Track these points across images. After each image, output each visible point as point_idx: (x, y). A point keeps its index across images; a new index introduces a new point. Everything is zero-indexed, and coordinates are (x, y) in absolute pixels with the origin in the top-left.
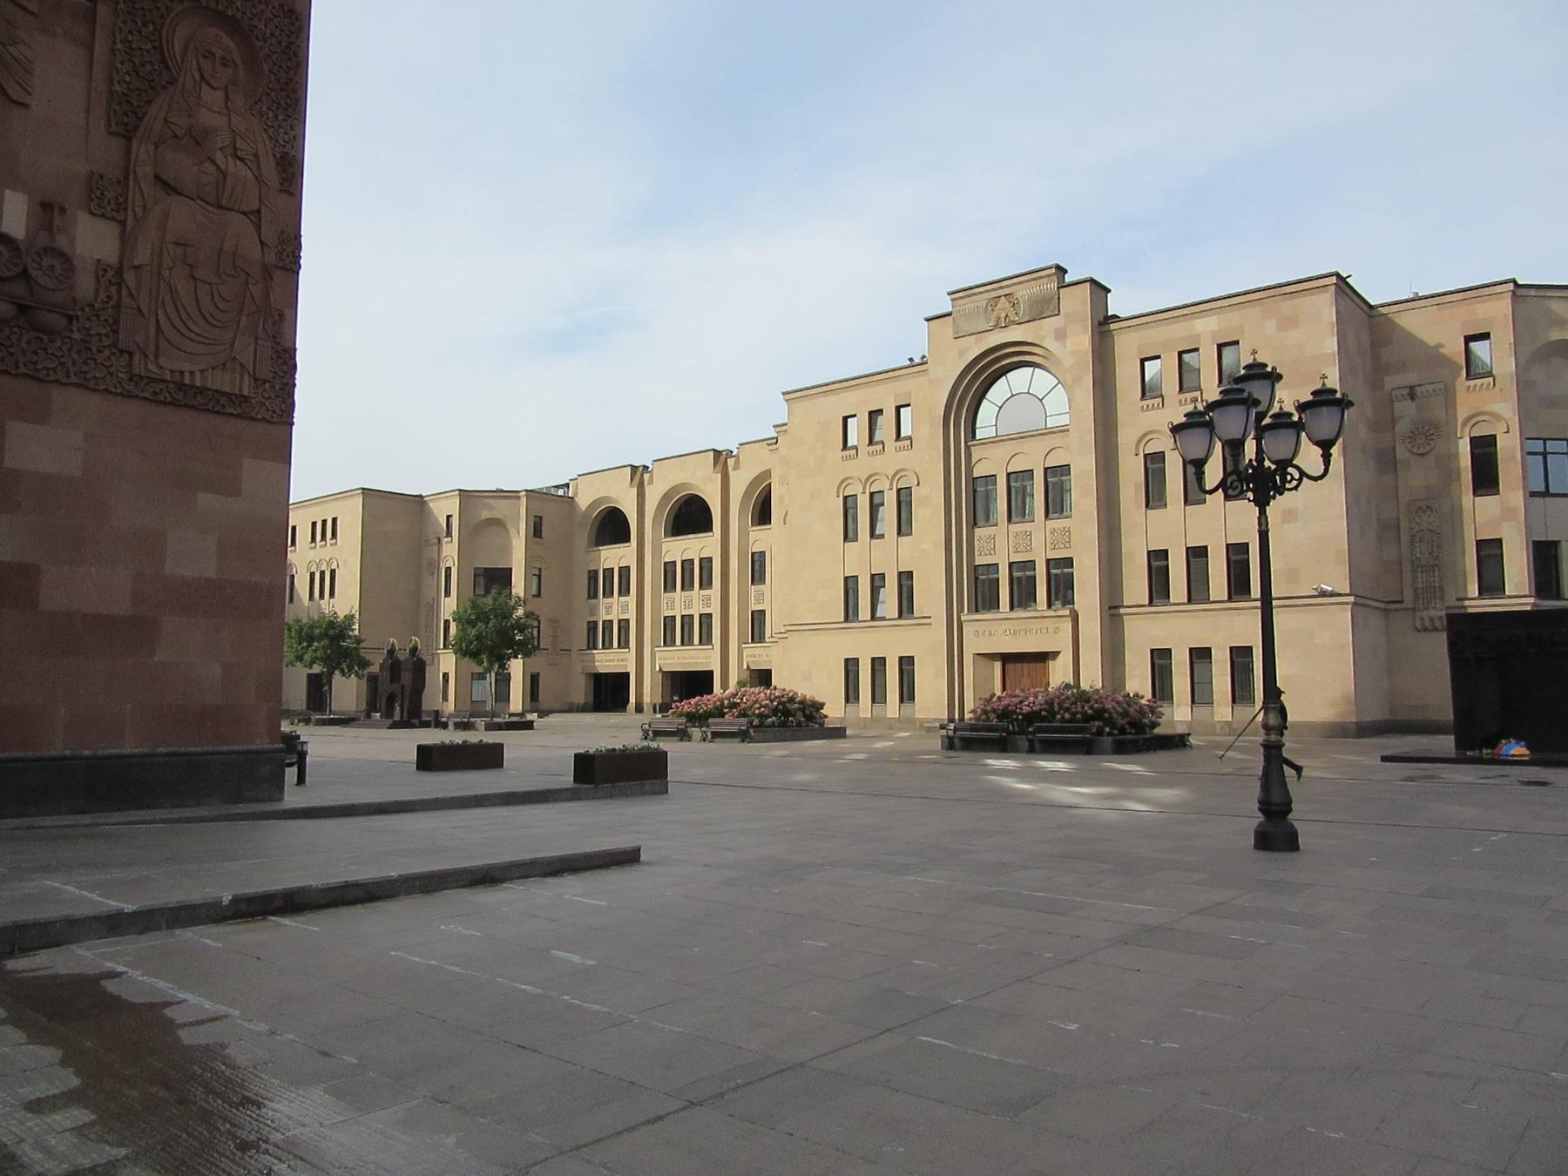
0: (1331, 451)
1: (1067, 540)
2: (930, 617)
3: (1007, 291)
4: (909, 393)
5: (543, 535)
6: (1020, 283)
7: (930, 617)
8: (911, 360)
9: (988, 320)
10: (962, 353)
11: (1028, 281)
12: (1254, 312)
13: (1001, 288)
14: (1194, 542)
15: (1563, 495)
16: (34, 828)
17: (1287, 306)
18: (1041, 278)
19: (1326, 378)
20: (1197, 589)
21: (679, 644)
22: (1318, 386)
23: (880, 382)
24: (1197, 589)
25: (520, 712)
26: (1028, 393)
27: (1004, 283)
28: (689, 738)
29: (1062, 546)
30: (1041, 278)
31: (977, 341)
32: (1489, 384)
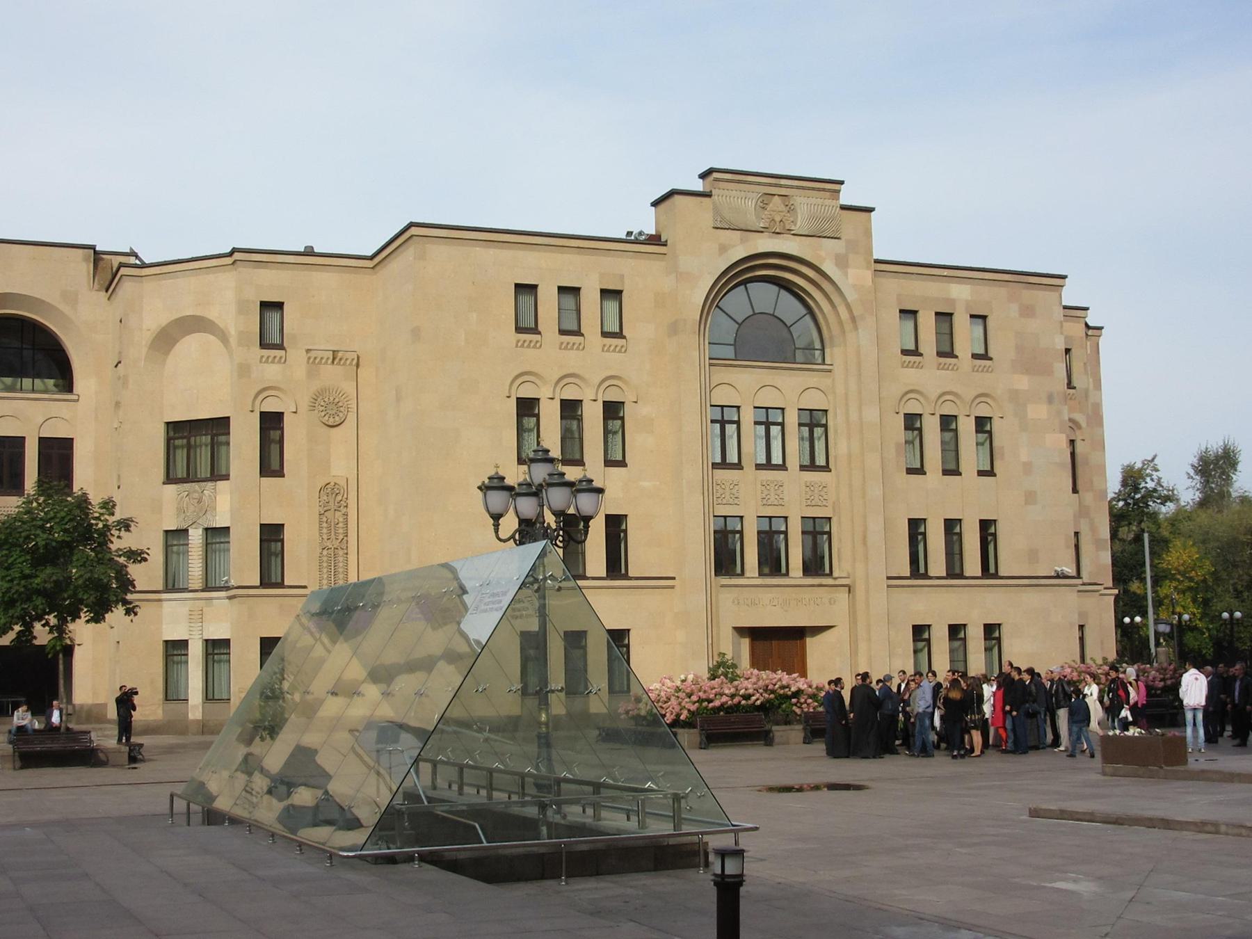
1: (725, 501)
2: (674, 578)
3: (783, 191)
4: (622, 276)
5: (956, 352)
6: (798, 187)
7: (674, 578)
9: (759, 218)
10: (723, 249)
11: (809, 189)
12: (1002, 291)
13: (781, 186)
14: (1072, 439)
15: (2, 417)
17: (1028, 295)
18: (824, 190)
19: (498, 467)
20: (772, 563)
21: (603, 572)
22: (492, 473)
23: (382, 265)
24: (772, 563)
25: (964, 574)
26: (740, 325)
27: (783, 182)
28: (830, 683)
29: (764, 496)
30: (824, 190)
31: (742, 241)
32: (281, 358)
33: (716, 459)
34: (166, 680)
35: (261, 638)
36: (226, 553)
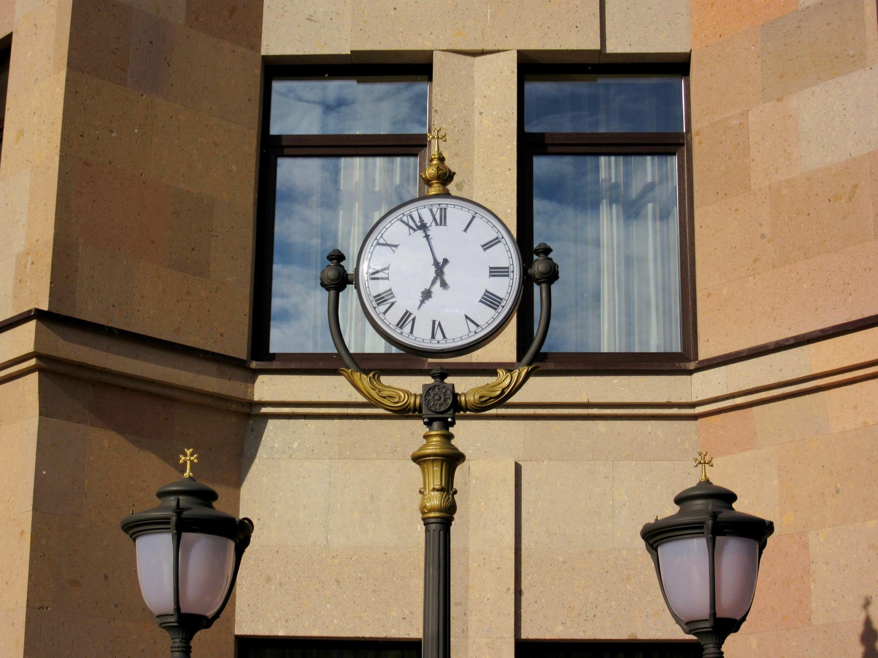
0: (349, 53)
8: (304, 52)
16: (433, 472)
33: (358, 163)
34: (487, 338)
35: (552, 251)
36: (547, 142)
